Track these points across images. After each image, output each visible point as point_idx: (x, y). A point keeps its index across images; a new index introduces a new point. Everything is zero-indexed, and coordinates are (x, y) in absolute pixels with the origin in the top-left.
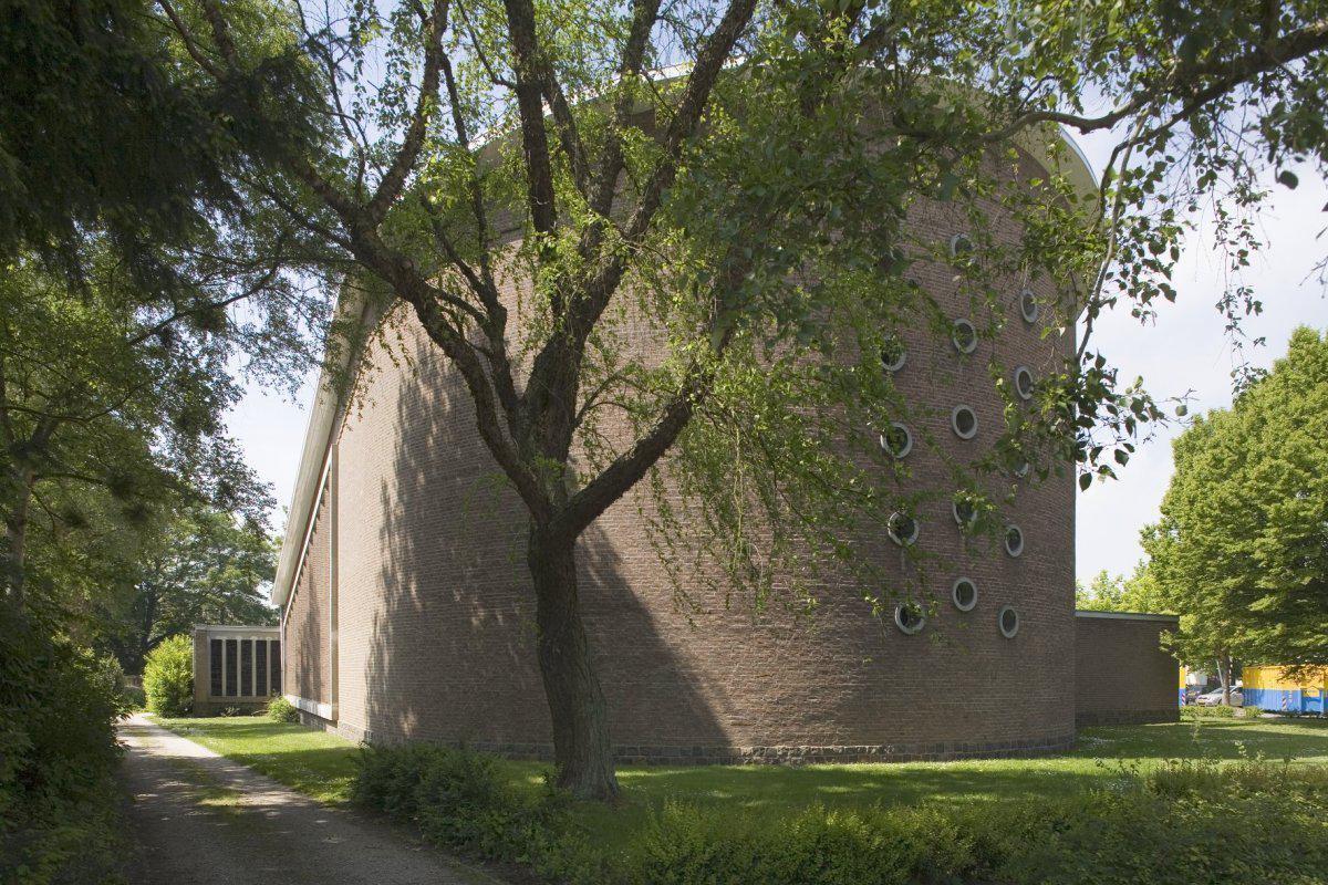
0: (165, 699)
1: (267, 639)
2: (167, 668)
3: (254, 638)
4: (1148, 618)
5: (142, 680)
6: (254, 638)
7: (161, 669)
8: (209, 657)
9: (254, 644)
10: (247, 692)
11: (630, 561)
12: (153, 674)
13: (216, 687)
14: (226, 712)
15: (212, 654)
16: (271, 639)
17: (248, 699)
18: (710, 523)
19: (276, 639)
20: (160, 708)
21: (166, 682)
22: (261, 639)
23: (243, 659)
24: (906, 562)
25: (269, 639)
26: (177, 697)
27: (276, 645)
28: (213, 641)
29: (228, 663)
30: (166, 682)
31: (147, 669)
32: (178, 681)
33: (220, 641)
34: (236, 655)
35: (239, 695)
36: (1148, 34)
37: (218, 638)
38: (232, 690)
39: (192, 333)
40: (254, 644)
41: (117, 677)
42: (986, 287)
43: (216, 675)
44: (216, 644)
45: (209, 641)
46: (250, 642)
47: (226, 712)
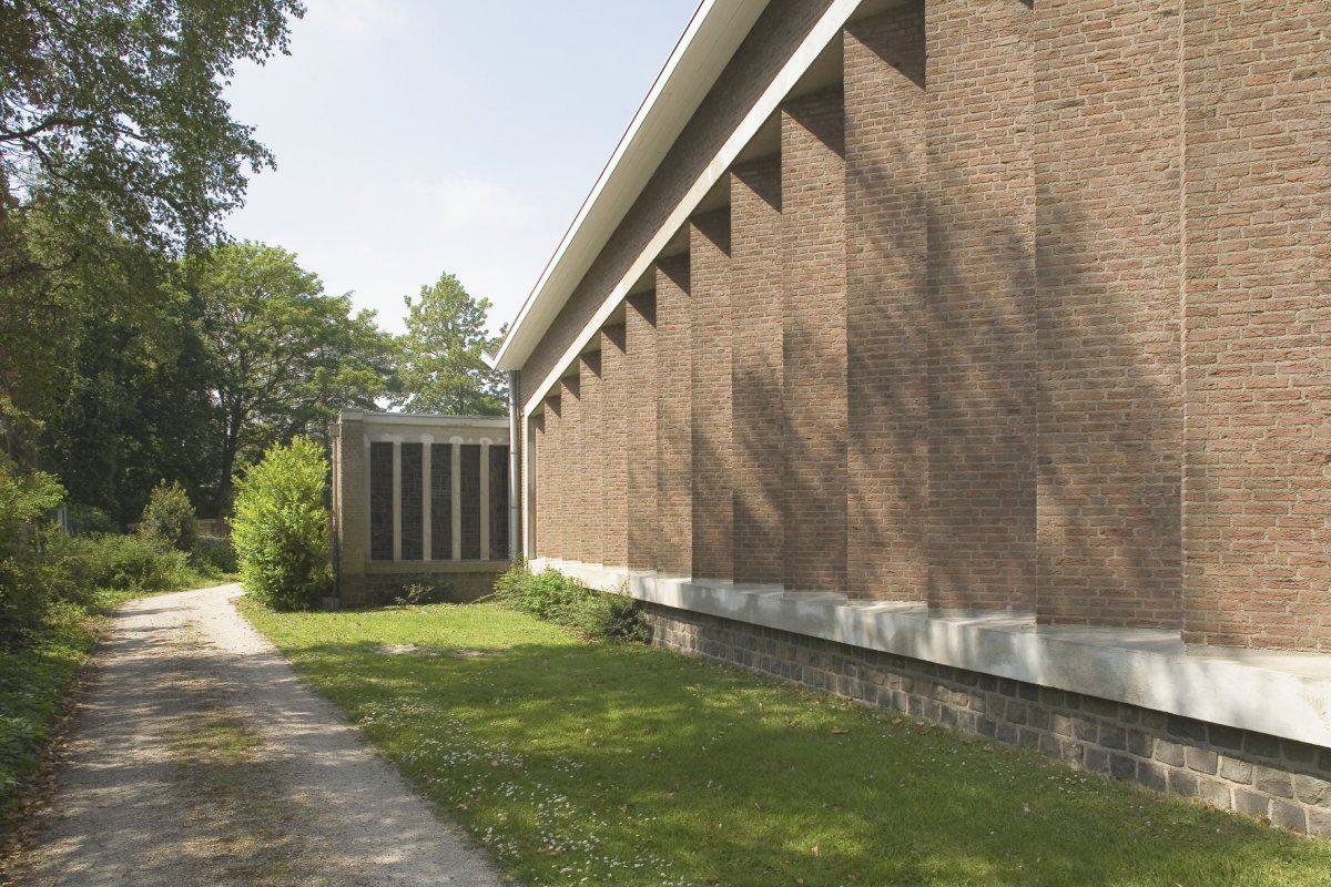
0: (279, 571)
1: (481, 442)
2: (284, 501)
3: (457, 441)
4: (391, 421)
5: (229, 529)
6: (457, 441)
7: (269, 505)
8: (368, 481)
9: (456, 453)
10: (471, 550)
11: (803, 305)
12: (251, 514)
13: (382, 547)
14: (404, 594)
15: (374, 474)
16: (490, 442)
17: (442, 566)
18: (1246, 199)
19: (500, 441)
20: (269, 588)
21: (282, 531)
22: (470, 441)
23: (434, 485)
24: (1178, 299)
25: (486, 442)
26: (306, 567)
27: (500, 455)
28: (375, 445)
29: (406, 491)
30: (282, 531)
31: (240, 505)
32: (307, 529)
33: (390, 445)
34: (420, 475)
35: (485, 556)
36: (96, 126)
37: (386, 438)
38: (412, 549)
39: (45, 116)
40: (456, 453)
41: (184, 523)
42: (42, 236)
43: (381, 519)
44: (382, 451)
45: (367, 445)
46: (449, 447)
47: (404, 594)
